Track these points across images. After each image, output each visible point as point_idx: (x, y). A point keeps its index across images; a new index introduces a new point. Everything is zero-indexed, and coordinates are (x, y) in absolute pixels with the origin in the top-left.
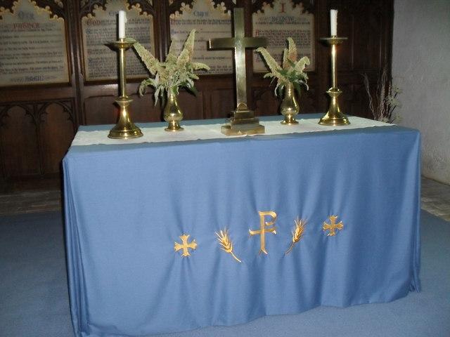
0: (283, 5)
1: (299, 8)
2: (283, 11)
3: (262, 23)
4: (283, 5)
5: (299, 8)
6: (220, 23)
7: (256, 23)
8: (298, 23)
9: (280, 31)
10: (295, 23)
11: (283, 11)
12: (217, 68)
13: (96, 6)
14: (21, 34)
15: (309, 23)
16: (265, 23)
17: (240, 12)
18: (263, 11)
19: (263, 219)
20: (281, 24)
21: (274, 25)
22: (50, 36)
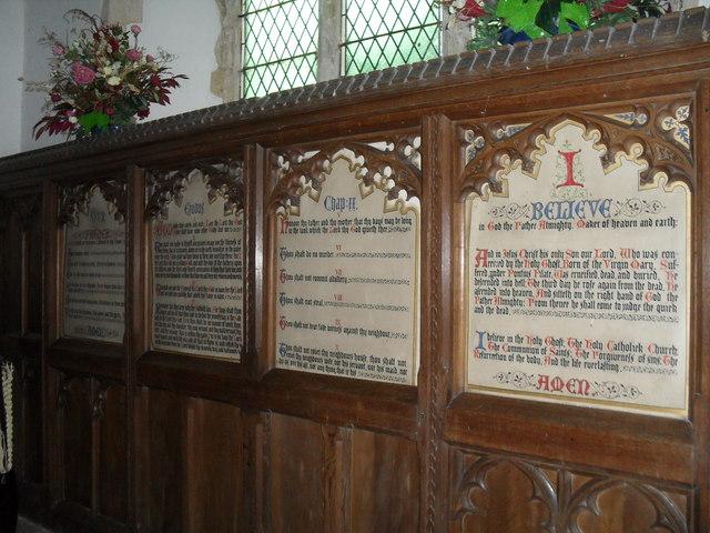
0: (569, 157)
1: (630, 164)
2: (570, 182)
3: (498, 227)
4: (569, 157)
5: (630, 164)
6: (382, 230)
7: (482, 227)
8: (627, 224)
9: (558, 254)
10: (616, 224)
11: (570, 182)
12: (368, 363)
13: (637, 149)
14: (95, 248)
15: (672, 222)
16: (507, 226)
17: (76, 259)
18: (496, 188)
19: (617, 45)
20: (560, 226)
21: (536, 233)
22: (108, 253)
